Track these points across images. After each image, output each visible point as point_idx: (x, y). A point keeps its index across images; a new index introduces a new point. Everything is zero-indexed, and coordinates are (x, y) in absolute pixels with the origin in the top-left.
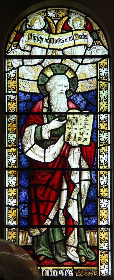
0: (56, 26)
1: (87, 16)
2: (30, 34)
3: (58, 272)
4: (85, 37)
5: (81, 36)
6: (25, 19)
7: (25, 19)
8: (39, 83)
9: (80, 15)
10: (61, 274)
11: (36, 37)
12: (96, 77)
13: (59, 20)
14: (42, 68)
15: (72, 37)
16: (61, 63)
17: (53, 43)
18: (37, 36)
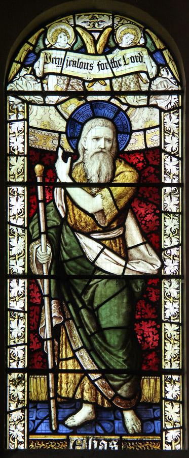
0: (95, 42)
1: (145, 28)
2: (132, 57)
3: (108, 445)
4: (140, 59)
5: (54, 60)
6: (43, 29)
7: (43, 29)
8: (69, 136)
9: (138, 26)
10: (114, 448)
11: (76, 62)
12: (160, 126)
13: (101, 32)
14: (124, 110)
15: (62, 59)
16: (109, 102)
17: (104, 69)
18: (77, 61)
